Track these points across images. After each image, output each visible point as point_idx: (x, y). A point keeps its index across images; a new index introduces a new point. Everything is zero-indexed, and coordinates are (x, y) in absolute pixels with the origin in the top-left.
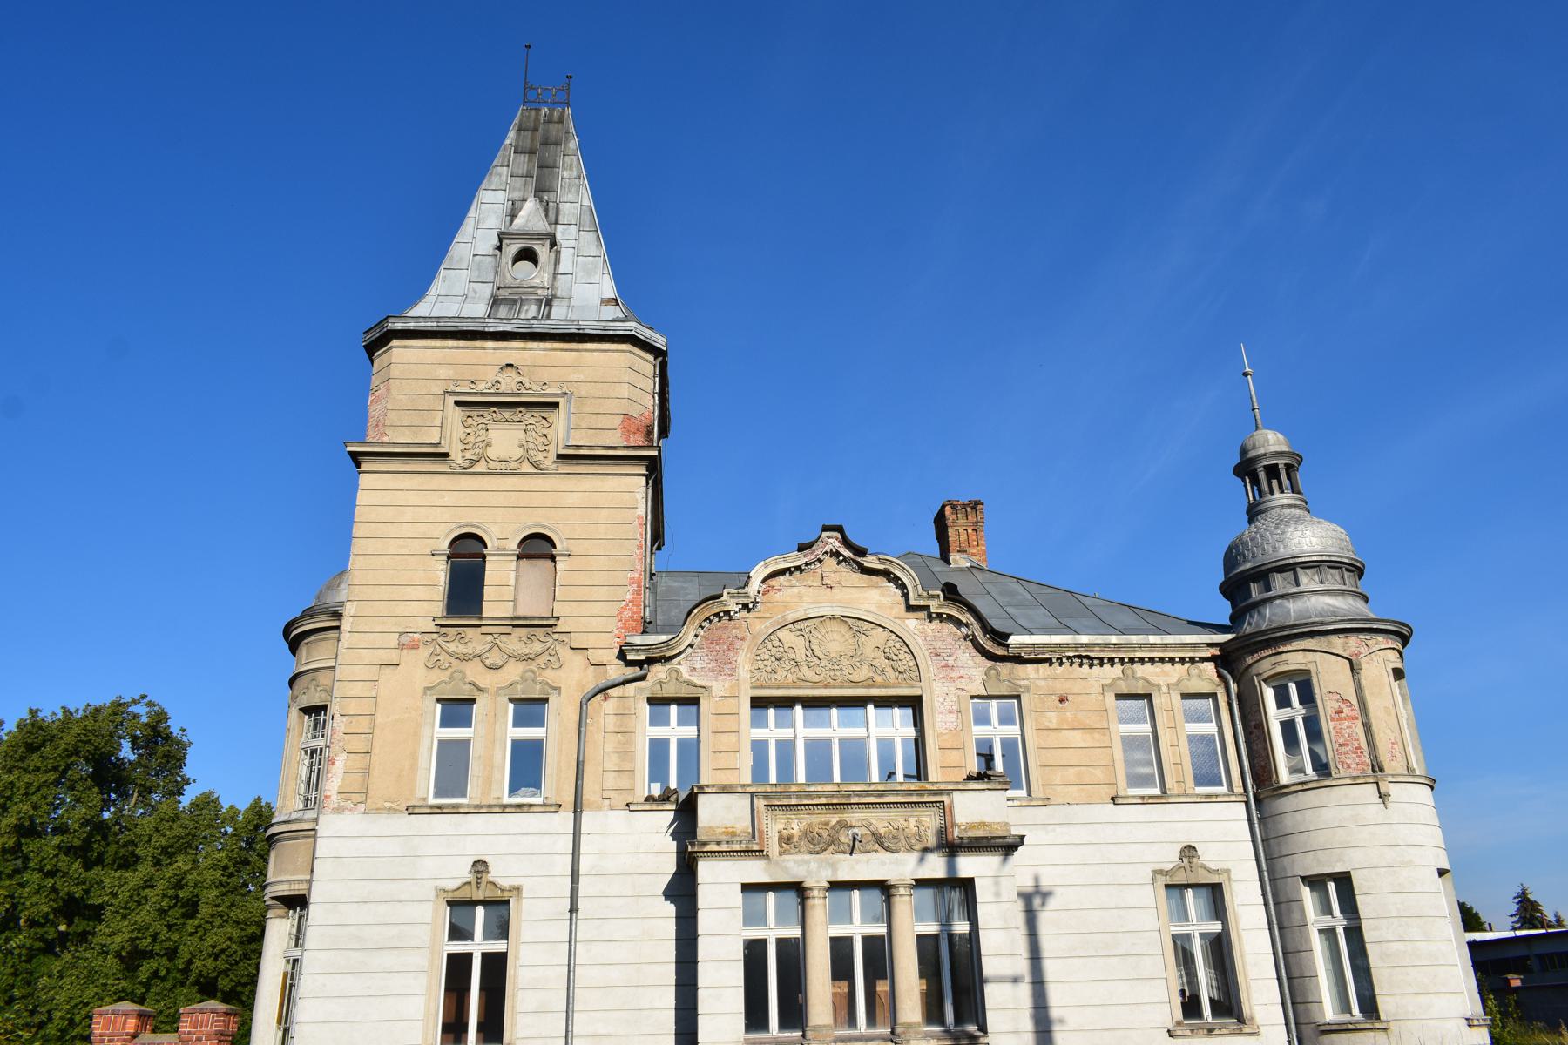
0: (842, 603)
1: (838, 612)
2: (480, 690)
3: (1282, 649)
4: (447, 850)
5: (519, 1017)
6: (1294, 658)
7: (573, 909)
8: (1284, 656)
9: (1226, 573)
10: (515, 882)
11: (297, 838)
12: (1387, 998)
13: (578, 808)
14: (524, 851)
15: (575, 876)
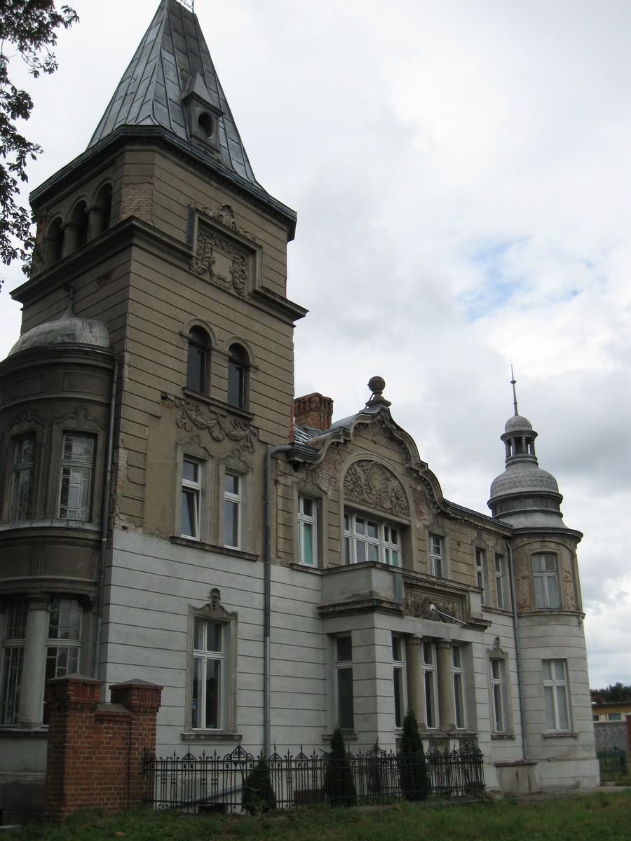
0: (382, 457)
1: (378, 460)
2: (210, 455)
3: (547, 539)
4: (200, 575)
5: (238, 708)
6: (602, 605)
7: (266, 633)
8: (546, 544)
9: (23, 331)
10: (234, 609)
11: (62, 543)
12: (576, 722)
13: (266, 560)
14: (239, 585)
15: (267, 610)
